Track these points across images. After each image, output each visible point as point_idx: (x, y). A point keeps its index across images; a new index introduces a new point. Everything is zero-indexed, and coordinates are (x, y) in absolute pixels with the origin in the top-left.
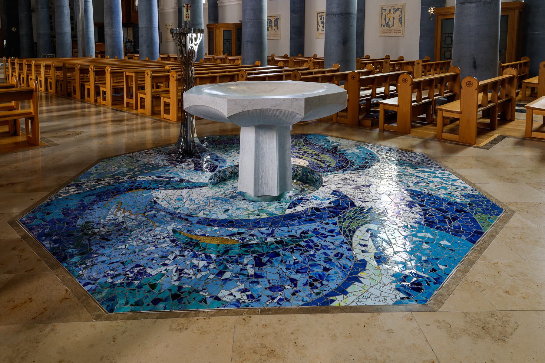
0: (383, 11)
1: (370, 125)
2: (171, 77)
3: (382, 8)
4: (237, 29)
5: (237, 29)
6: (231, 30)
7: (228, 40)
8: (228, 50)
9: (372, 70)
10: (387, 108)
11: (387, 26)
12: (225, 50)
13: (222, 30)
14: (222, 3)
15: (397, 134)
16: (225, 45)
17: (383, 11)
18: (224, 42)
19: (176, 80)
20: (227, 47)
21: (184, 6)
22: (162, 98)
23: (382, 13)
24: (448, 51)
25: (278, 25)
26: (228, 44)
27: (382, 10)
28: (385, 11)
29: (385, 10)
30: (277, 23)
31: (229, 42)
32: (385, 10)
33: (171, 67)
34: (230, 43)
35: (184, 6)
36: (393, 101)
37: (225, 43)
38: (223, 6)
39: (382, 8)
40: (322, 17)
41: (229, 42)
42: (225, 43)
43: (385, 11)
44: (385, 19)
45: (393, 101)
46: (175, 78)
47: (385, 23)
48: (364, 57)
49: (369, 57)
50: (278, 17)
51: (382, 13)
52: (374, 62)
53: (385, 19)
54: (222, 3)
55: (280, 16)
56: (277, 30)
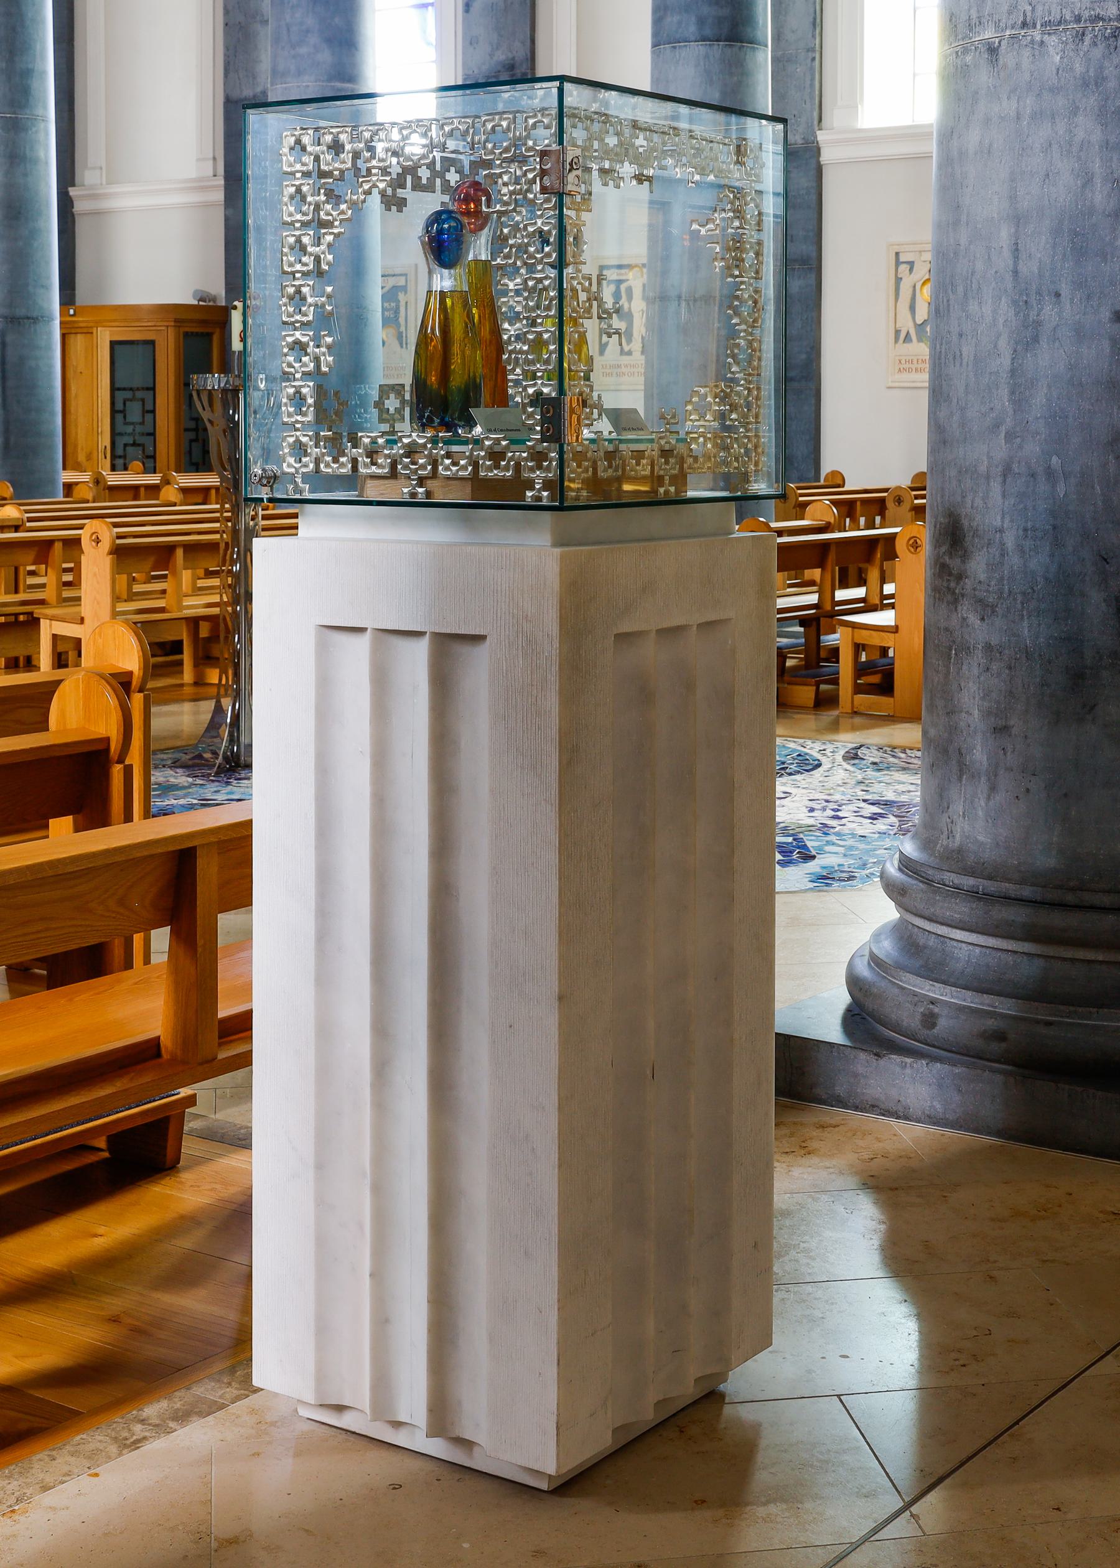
0: (903, 268)
1: (811, 703)
2: (85, 543)
3: (897, 254)
4: (186, 334)
5: (186, 334)
6: (152, 343)
7: (139, 394)
8: (134, 444)
9: (829, 523)
10: (863, 637)
11: (920, 340)
12: (121, 441)
13: (104, 337)
14: (95, 197)
15: (893, 721)
16: (120, 417)
17: (903, 268)
18: (113, 404)
19: (110, 553)
20: (129, 429)
21: (235, 308)
22: (44, 624)
23: (898, 280)
24: (133, 424)
25: (402, 320)
26: (134, 412)
27: (898, 263)
28: (911, 270)
29: (911, 264)
30: (397, 311)
31: (143, 400)
32: (911, 264)
33: (27, 512)
34: (149, 407)
35: (235, 308)
36: (885, 618)
37: (119, 406)
38: (98, 213)
39: (897, 254)
40: (623, 287)
41: (143, 400)
42: (119, 406)
43: (911, 270)
44: (912, 308)
45: (885, 618)
46: (106, 545)
47: (911, 324)
48: (822, 482)
49: (840, 482)
50: (401, 282)
51: (898, 280)
52: (853, 502)
53: (912, 308)
54: (95, 197)
55: (411, 277)
56: (396, 343)
